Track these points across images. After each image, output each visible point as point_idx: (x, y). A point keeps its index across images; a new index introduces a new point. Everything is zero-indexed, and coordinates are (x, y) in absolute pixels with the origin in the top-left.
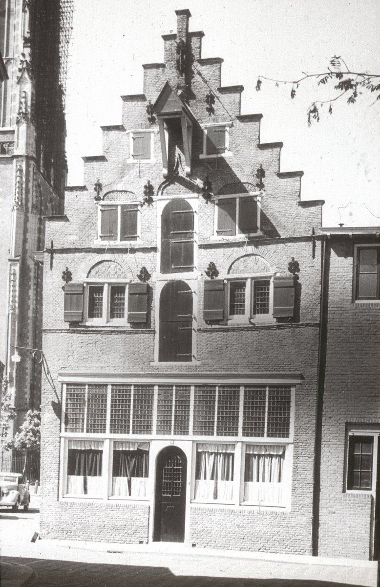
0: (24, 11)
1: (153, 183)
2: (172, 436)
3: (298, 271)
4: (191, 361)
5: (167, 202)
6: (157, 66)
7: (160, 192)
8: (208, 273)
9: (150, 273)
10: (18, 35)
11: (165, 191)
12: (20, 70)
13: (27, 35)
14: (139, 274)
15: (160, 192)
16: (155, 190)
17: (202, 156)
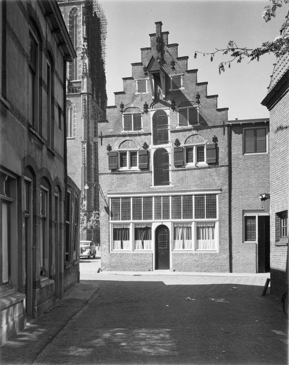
0: (83, 25)
1: (148, 103)
2: (162, 220)
3: (217, 141)
4: (169, 185)
5: (155, 112)
6: (148, 49)
7: (151, 107)
8: (175, 144)
9: (148, 145)
10: (80, 36)
11: (154, 106)
12: (82, 53)
13: (85, 36)
15: (151, 107)
16: (149, 106)
17: (171, 90)
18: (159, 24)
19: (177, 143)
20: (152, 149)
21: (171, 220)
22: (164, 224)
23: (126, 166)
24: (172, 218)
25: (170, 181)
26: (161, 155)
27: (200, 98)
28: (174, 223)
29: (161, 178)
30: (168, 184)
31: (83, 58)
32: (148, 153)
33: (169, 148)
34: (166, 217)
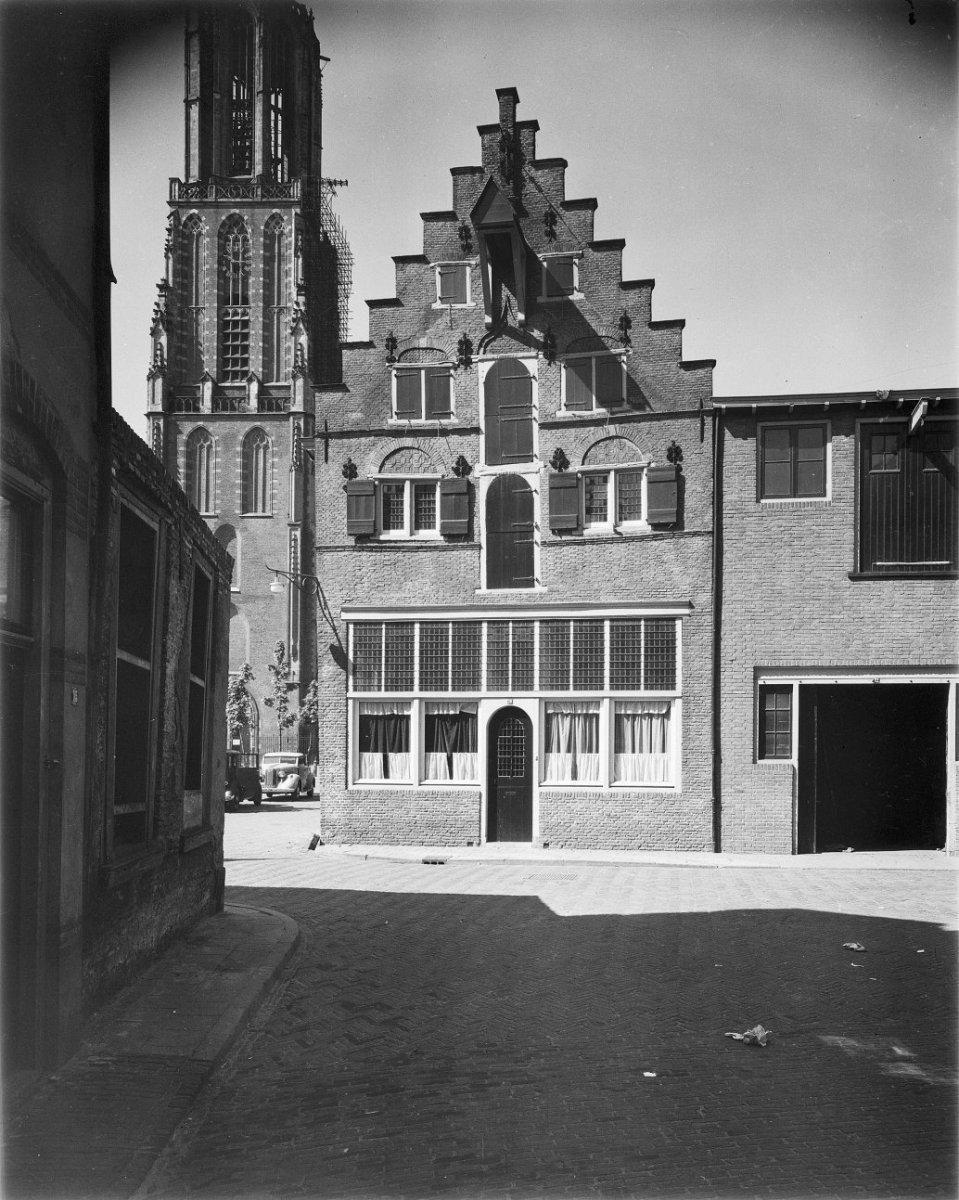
1: (471, 337)
3: (681, 459)
4: (533, 586)
7: (482, 350)
8: (554, 464)
9: (470, 464)
12: (294, 320)
14: (454, 465)
15: (482, 350)
16: (475, 347)
17: (541, 300)
18: (508, 97)
19: (560, 460)
20: (484, 476)
21: (537, 692)
22: (517, 703)
23: (402, 527)
24: (542, 687)
25: (537, 574)
26: (510, 499)
27: (630, 327)
28: (546, 703)
29: (510, 565)
30: (530, 583)
31: (295, 332)
32: (471, 489)
33: (535, 474)
34: (524, 682)
